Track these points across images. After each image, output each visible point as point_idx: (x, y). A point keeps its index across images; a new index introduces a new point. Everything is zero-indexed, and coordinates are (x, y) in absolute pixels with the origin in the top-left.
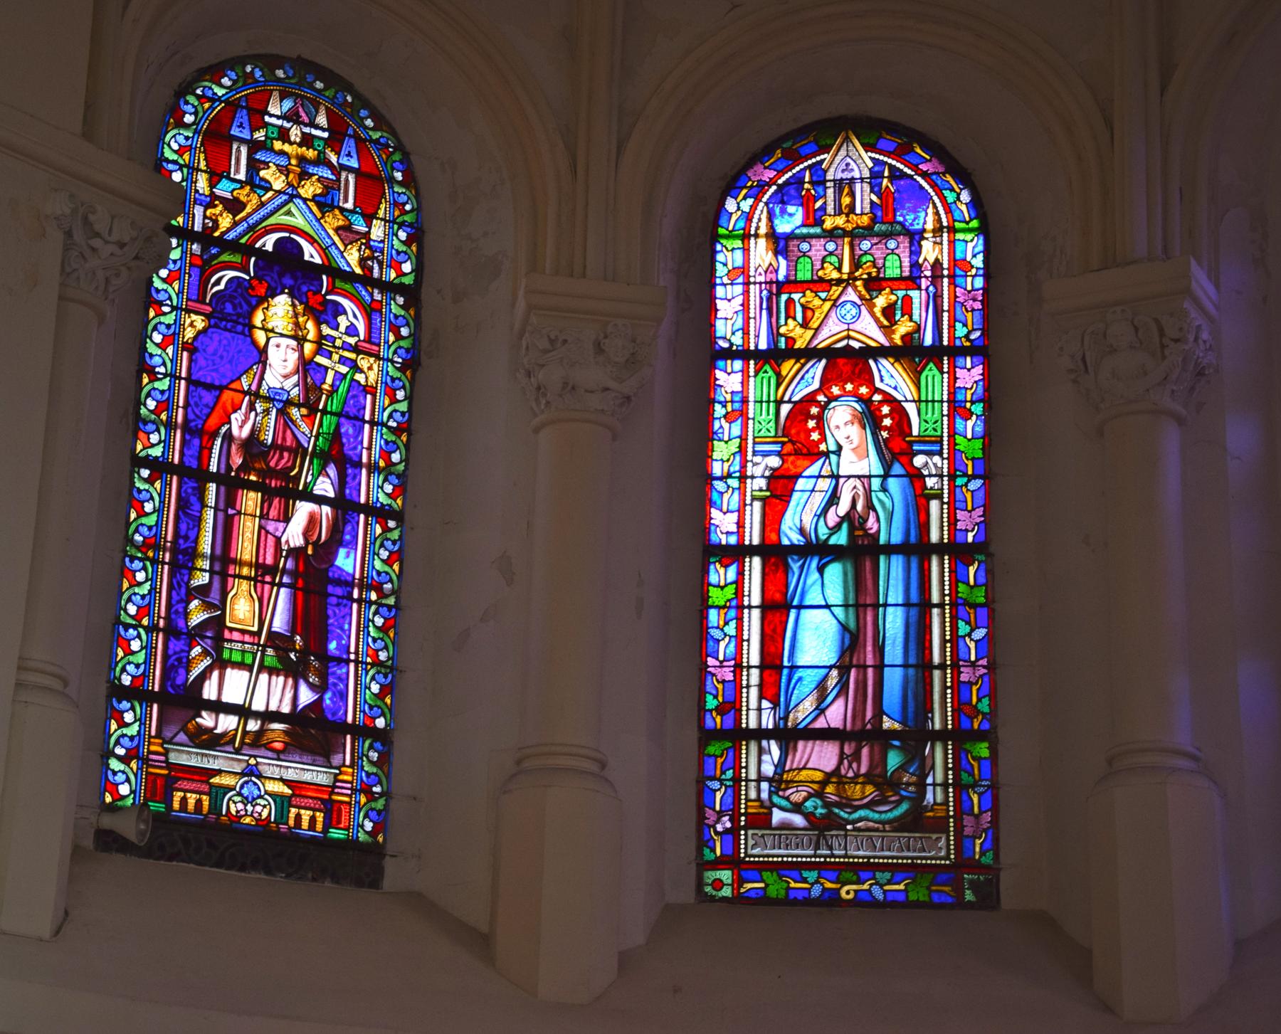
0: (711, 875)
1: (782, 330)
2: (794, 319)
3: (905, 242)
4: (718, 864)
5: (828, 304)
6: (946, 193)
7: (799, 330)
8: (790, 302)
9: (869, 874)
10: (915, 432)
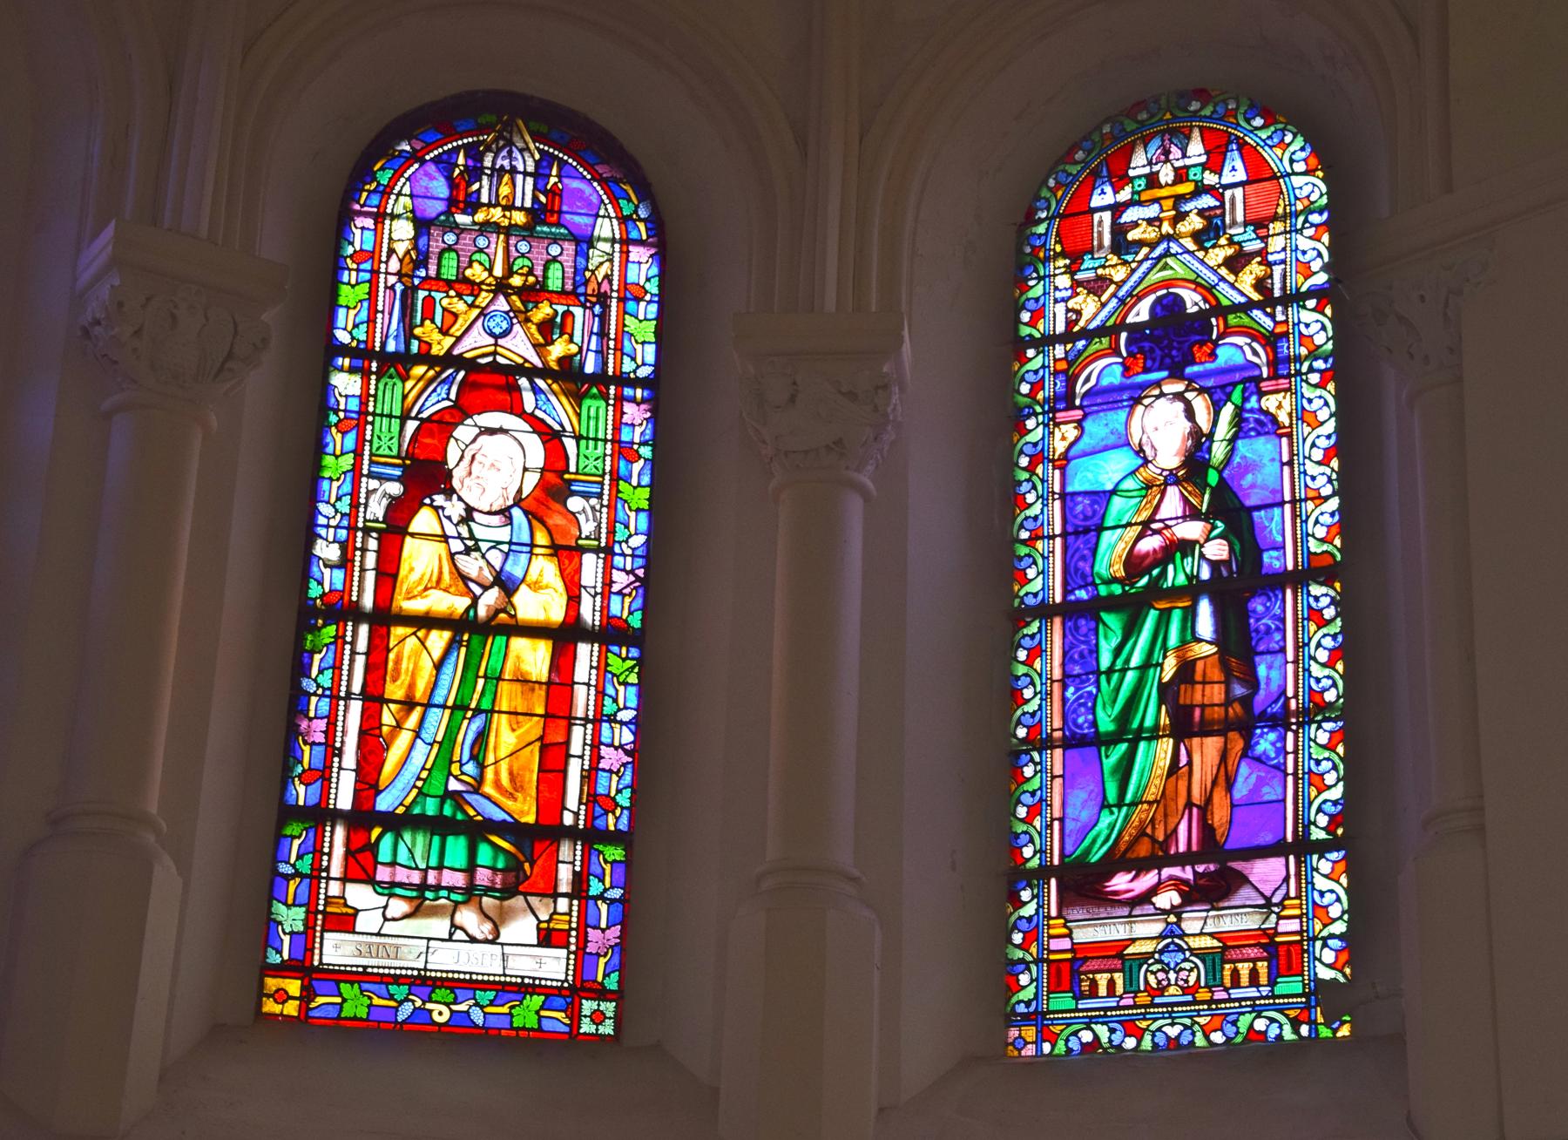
0: (272, 983)
1: (417, 331)
2: (433, 321)
3: (570, 248)
4: (283, 970)
5: (476, 312)
6: (623, 203)
7: (436, 336)
8: (429, 303)
9: (470, 993)
10: (572, 468)
